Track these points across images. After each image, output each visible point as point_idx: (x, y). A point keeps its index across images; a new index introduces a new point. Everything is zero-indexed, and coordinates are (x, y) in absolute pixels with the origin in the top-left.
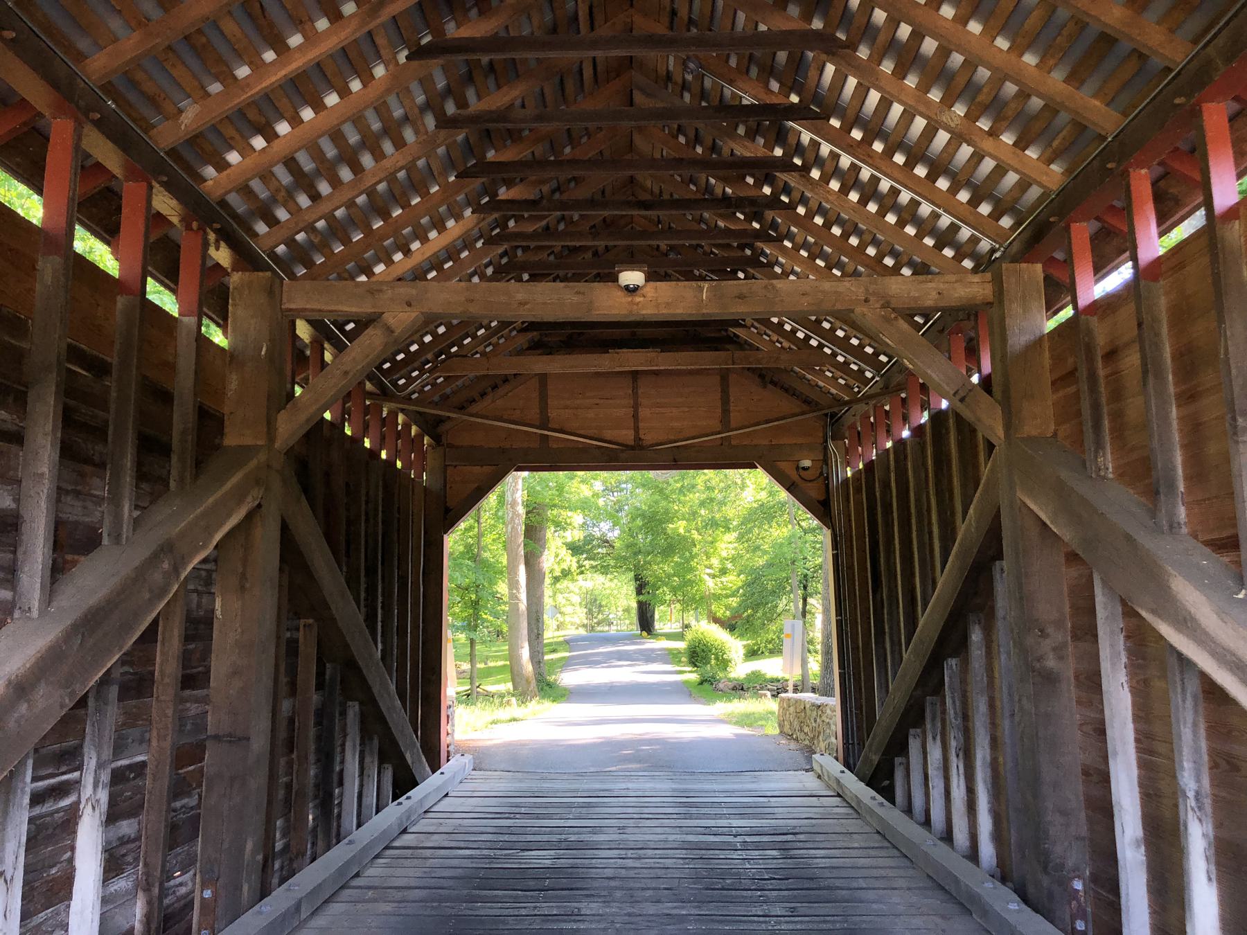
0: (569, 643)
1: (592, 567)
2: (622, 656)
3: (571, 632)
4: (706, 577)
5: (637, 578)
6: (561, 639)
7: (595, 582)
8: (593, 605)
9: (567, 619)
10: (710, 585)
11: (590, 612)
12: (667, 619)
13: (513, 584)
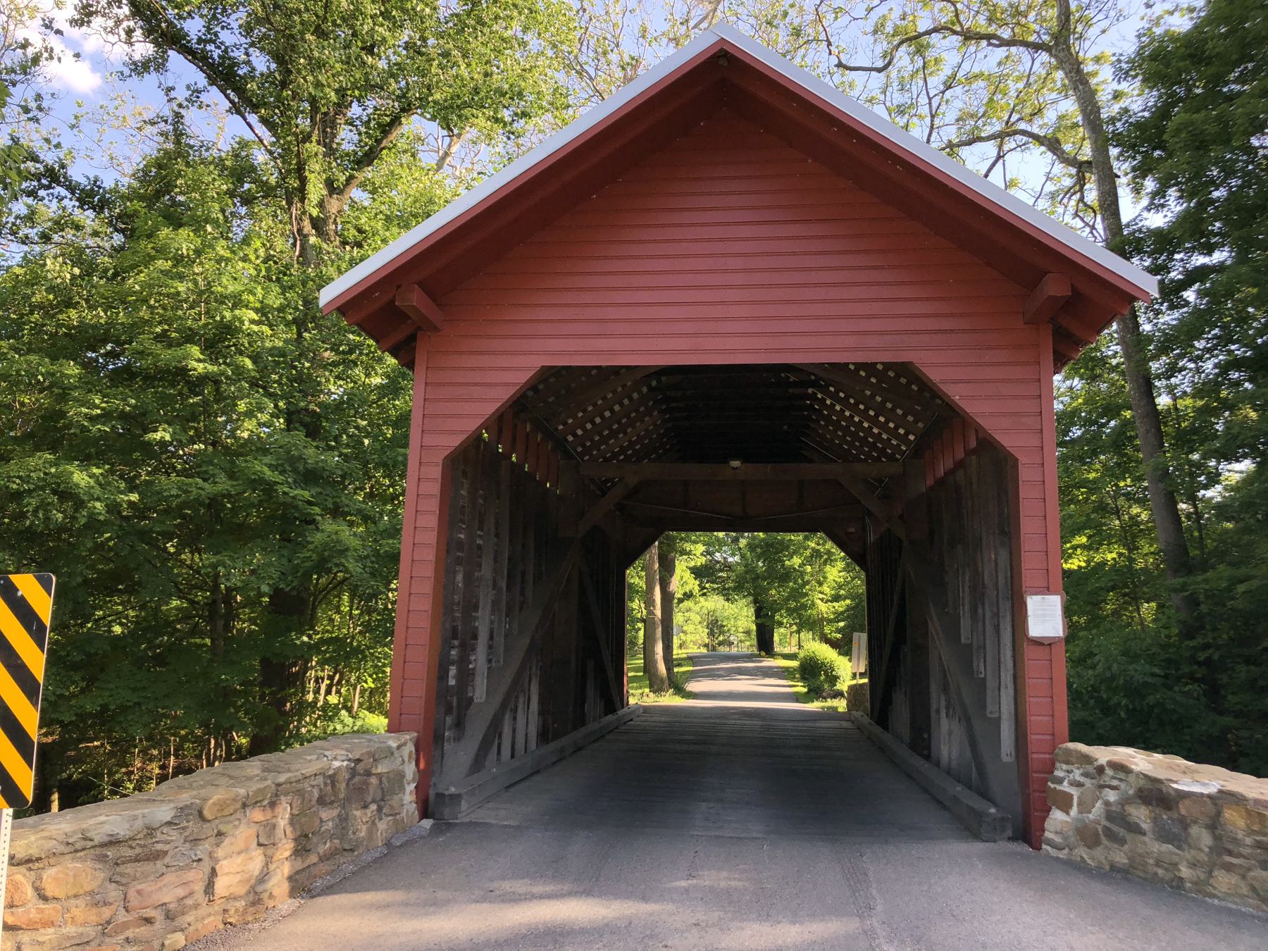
0: (692, 659)
1: (714, 589)
2: (741, 672)
3: (694, 650)
4: (819, 602)
5: (755, 602)
6: (685, 656)
7: (715, 603)
8: (715, 626)
9: (689, 638)
10: (823, 608)
11: (711, 634)
12: (785, 639)
13: (649, 603)
